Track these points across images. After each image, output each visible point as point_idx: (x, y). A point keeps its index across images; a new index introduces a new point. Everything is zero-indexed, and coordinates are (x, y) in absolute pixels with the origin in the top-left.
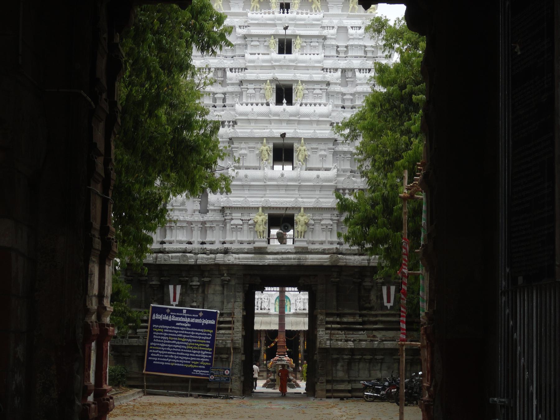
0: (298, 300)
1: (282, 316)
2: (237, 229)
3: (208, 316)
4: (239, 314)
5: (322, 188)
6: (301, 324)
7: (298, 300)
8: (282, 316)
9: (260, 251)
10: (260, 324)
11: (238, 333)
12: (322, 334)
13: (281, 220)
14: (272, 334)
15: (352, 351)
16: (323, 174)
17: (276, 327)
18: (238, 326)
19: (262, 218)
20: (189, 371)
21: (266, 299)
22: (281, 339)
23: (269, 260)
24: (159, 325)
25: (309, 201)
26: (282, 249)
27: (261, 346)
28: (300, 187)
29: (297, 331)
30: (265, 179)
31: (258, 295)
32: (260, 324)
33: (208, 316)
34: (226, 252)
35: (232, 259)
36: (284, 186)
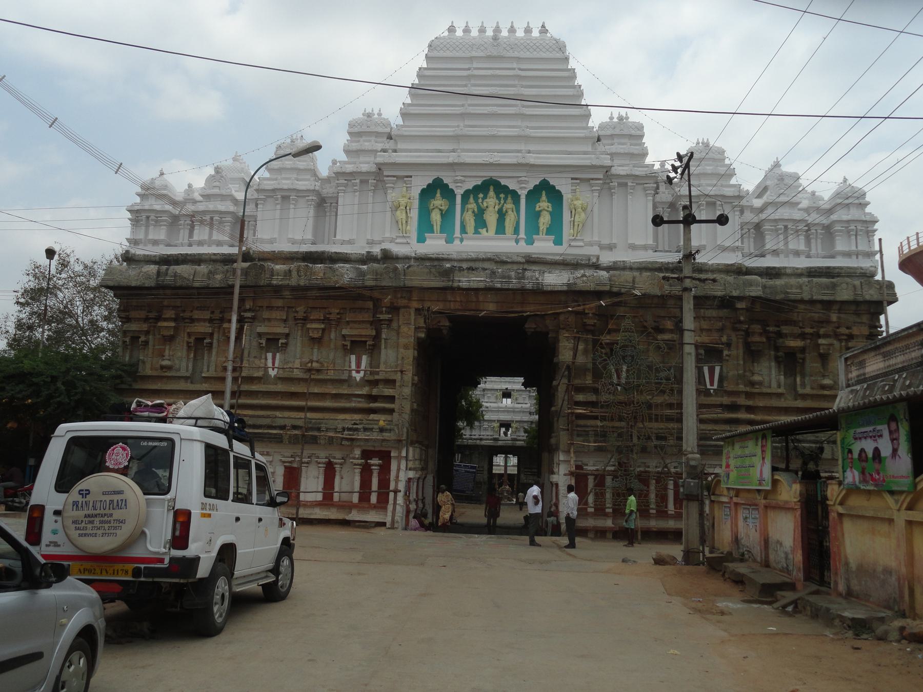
0: (513, 460)
1: (506, 466)
2: (485, 429)
3: (472, 468)
4: (486, 467)
5: (524, 412)
6: (513, 471)
7: (513, 460)
8: (506, 466)
9: (496, 440)
10: (496, 470)
11: (485, 476)
12: (522, 476)
13: (506, 425)
14: (501, 475)
15: (396, 287)
16: (524, 406)
17: (503, 472)
18: (486, 472)
19: (496, 425)
20: (463, 492)
21: (499, 460)
22: (505, 478)
23: (500, 443)
24: (153, 577)
25: (518, 418)
26: (506, 437)
27: (496, 481)
28: (514, 411)
29: (504, 227)
30: (499, 407)
31: (495, 458)
32: (496, 470)
33: (472, 468)
34: (481, 439)
35: (483, 443)
36: (507, 410)
